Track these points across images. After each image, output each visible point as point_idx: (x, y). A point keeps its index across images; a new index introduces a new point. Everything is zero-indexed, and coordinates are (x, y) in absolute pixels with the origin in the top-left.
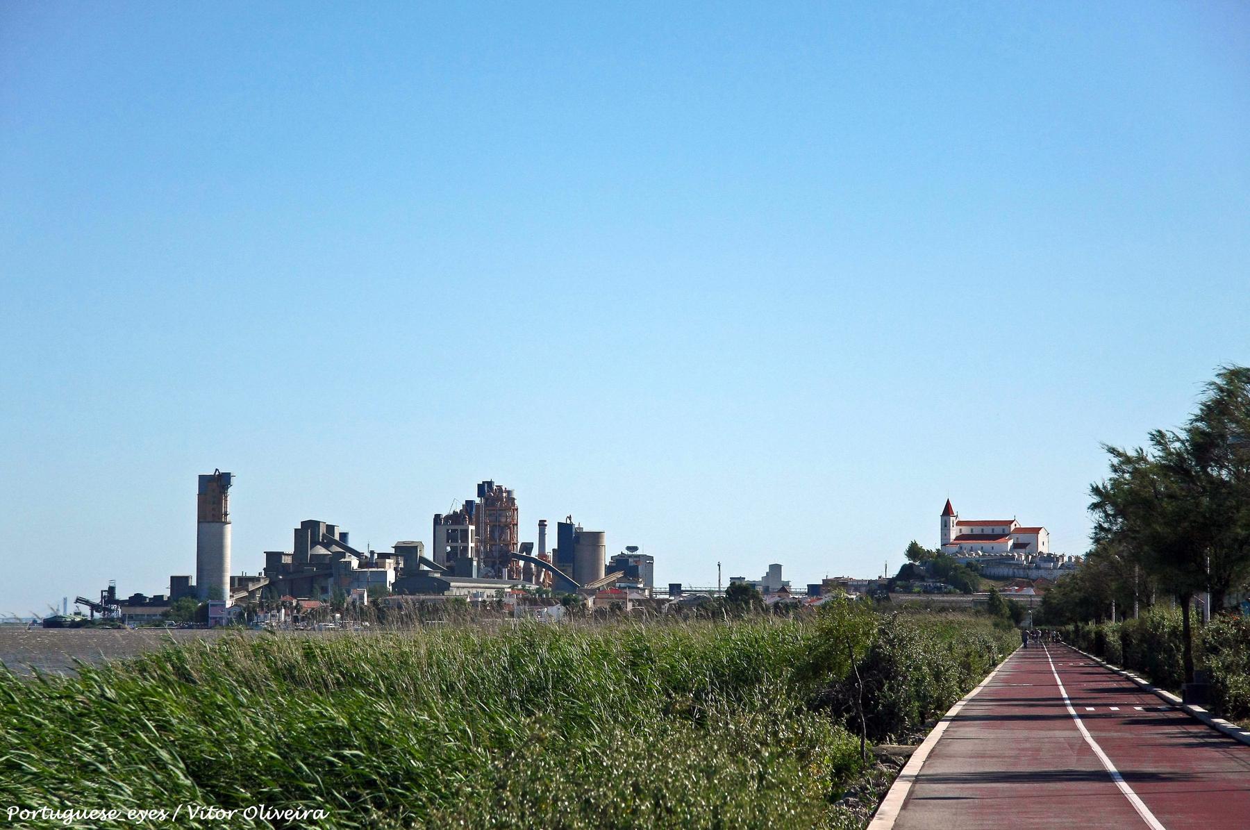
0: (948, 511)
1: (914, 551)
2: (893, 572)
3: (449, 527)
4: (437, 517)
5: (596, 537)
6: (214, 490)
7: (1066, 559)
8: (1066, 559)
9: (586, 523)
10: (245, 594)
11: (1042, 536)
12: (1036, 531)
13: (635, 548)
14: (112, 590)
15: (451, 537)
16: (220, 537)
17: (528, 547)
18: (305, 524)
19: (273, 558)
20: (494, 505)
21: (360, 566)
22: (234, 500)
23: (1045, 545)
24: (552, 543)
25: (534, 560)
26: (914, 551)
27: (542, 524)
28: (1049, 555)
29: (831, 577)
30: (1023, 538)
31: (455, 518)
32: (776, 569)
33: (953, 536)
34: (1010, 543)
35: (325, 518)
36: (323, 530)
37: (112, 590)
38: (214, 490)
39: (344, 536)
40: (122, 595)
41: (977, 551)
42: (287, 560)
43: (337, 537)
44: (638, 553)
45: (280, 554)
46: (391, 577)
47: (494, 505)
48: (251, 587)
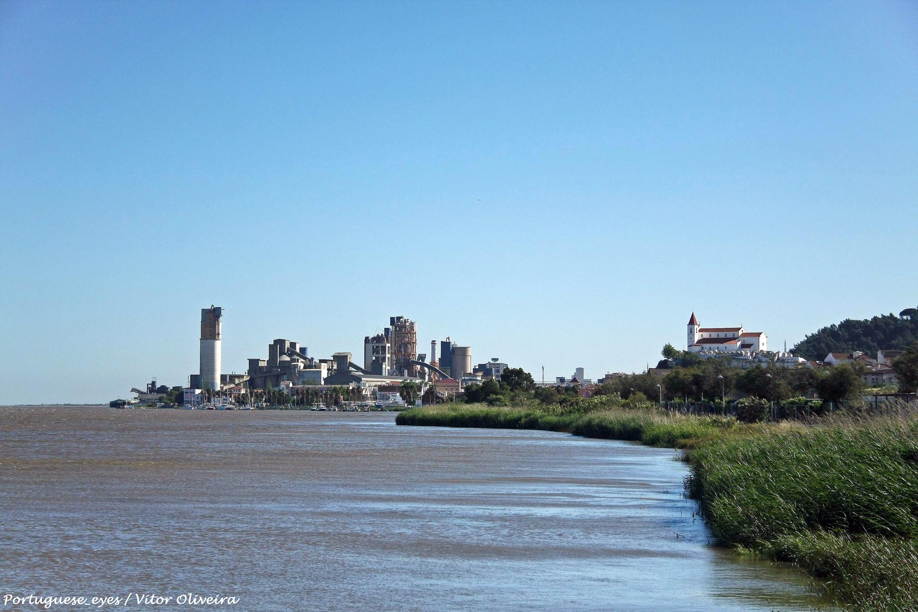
0: (692, 321)
1: (668, 351)
2: (654, 365)
3: (374, 345)
4: (367, 338)
5: (464, 350)
6: (211, 319)
7: (781, 355)
8: (781, 355)
9: (458, 341)
10: (232, 386)
11: (762, 339)
12: (758, 335)
13: (497, 359)
14: (153, 383)
15: (375, 351)
16: (212, 349)
17: (422, 357)
18: (276, 342)
19: (253, 363)
20: (401, 331)
21: (304, 368)
22: (222, 325)
23: (764, 345)
24: (438, 355)
25: (426, 365)
26: (668, 351)
27: (433, 343)
28: (768, 352)
29: (611, 373)
30: (748, 340)
31: (378, 339)
32: (580, 371)
33: (696, 340)
34: (739, 344)
35: (289, 338)
36: (287, 345)
37: (153, 383)
38: (211, 319)
39: (303, 350)
40: (158, 385)
41: (713, 350)
42: (261, 364)
43: (298, 350)
44: (498, 362)
45: (258, 360)
46: (324, 374)
47: (401, 331)
48: (237, 381)
